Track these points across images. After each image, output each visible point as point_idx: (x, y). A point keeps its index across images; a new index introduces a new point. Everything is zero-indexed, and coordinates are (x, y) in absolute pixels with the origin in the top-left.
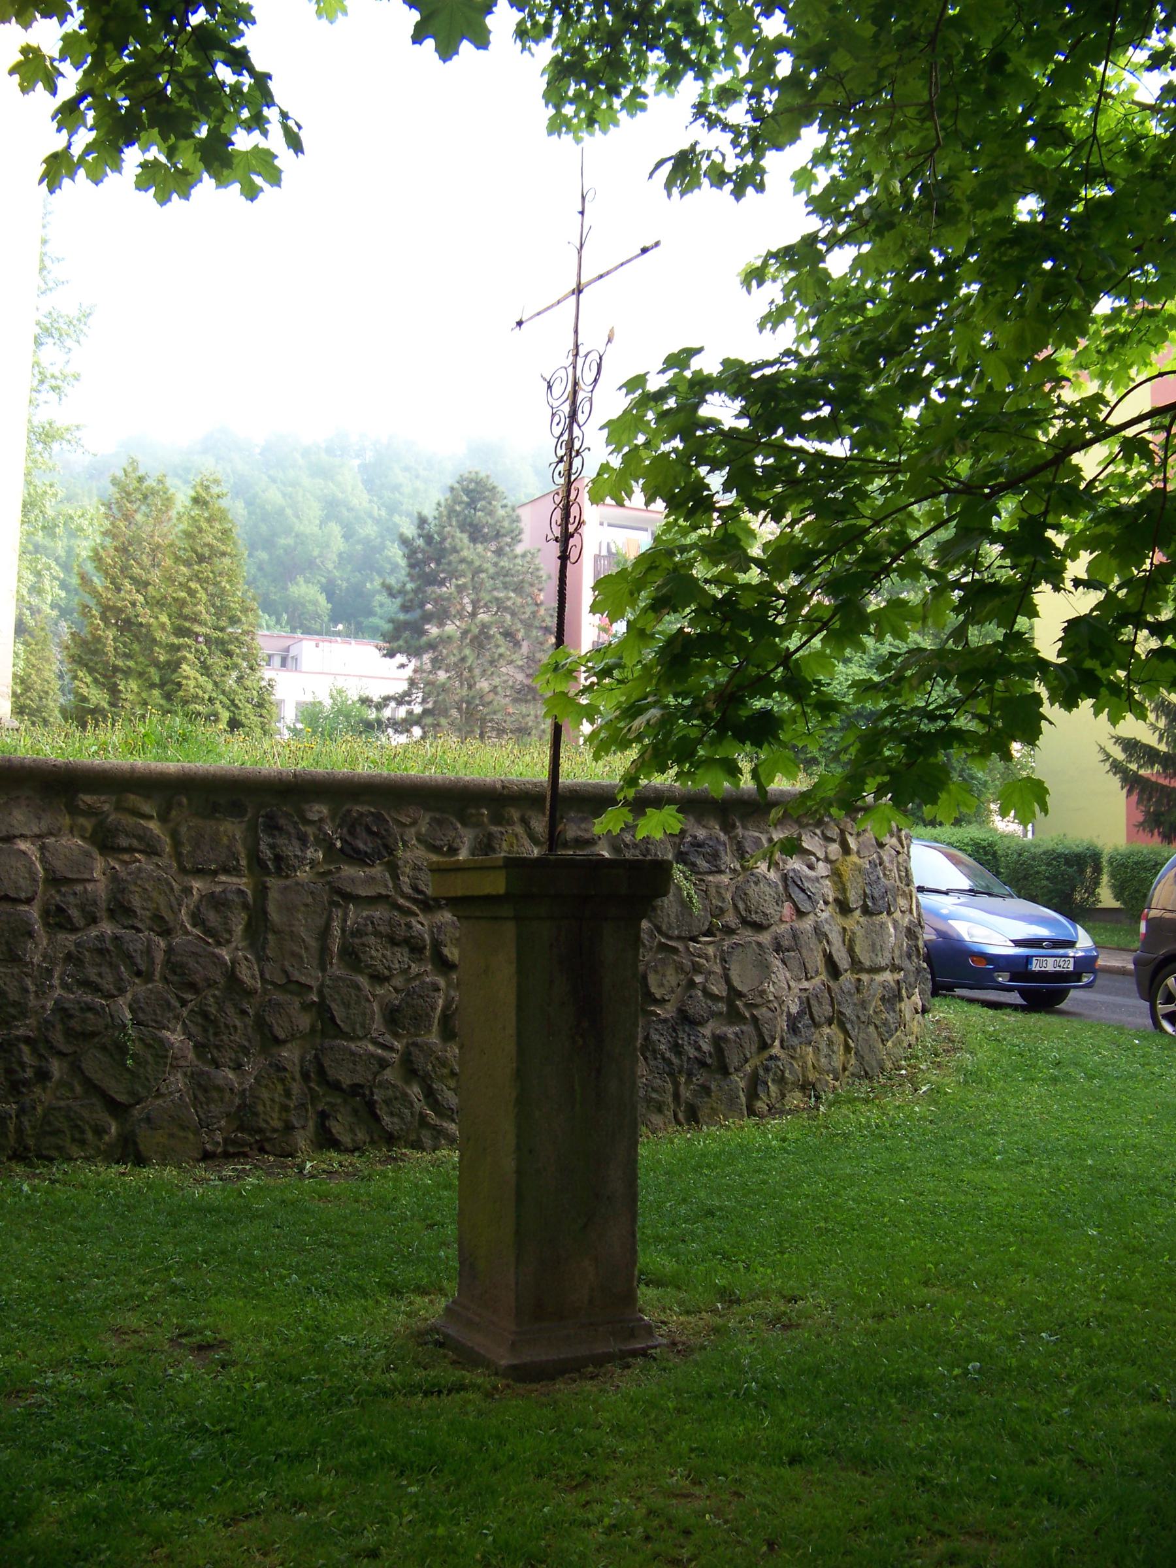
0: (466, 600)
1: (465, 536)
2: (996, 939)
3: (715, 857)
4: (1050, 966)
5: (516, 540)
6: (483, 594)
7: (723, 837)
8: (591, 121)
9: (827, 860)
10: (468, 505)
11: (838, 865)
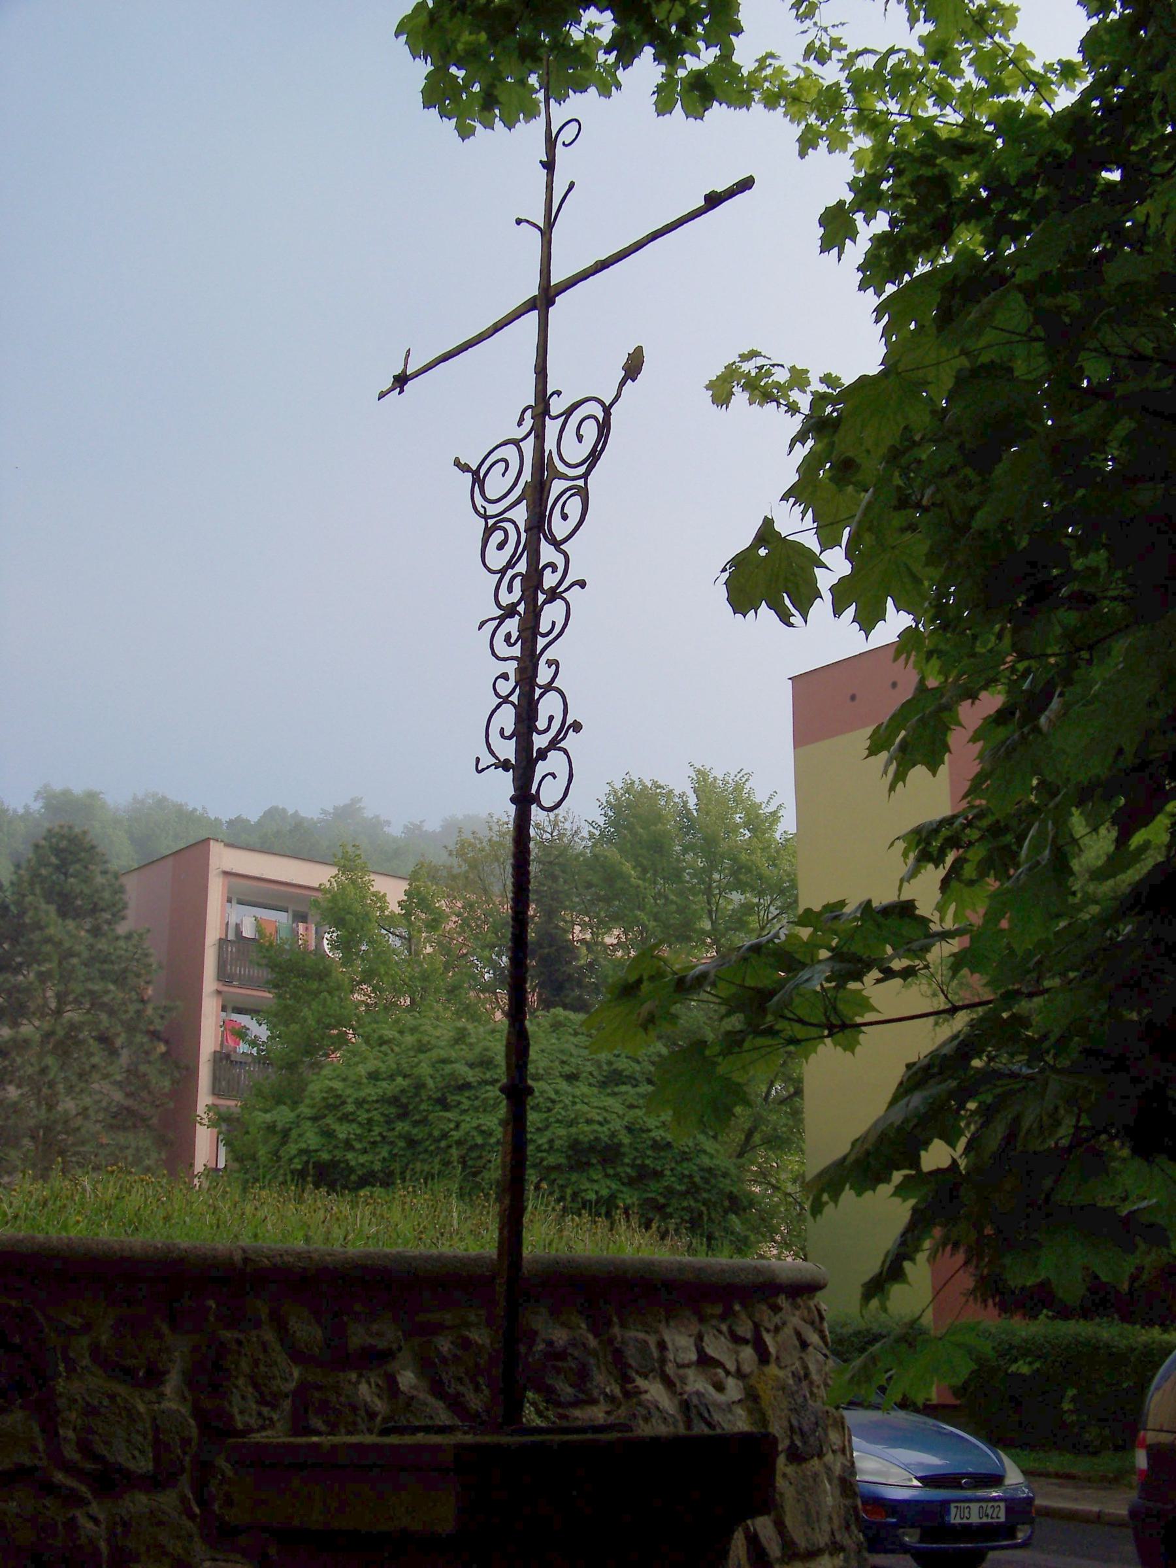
0: (50, 993)
1: (52, 908)
2: (897, 1475)
3: (582, 1376)
4: (974, 1516)
5: (118, 915)
6: (72, 985)
7: (592, 1342)
8: (489, 102)
9: (740, 1375)
10: (58, 868)
11: (752, 1381)
